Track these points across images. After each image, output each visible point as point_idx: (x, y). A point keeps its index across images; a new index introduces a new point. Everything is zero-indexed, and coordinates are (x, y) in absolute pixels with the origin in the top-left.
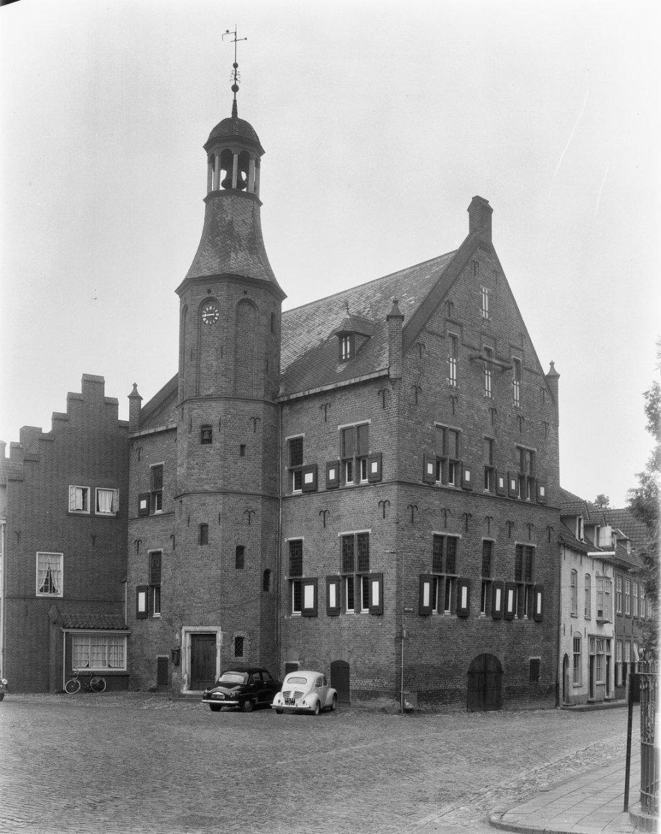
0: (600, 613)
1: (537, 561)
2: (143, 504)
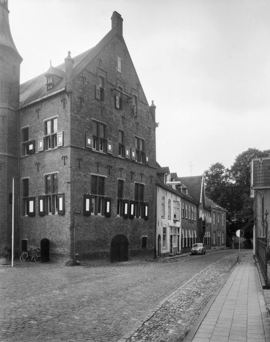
0: (175, 216)
1: (145, 191)
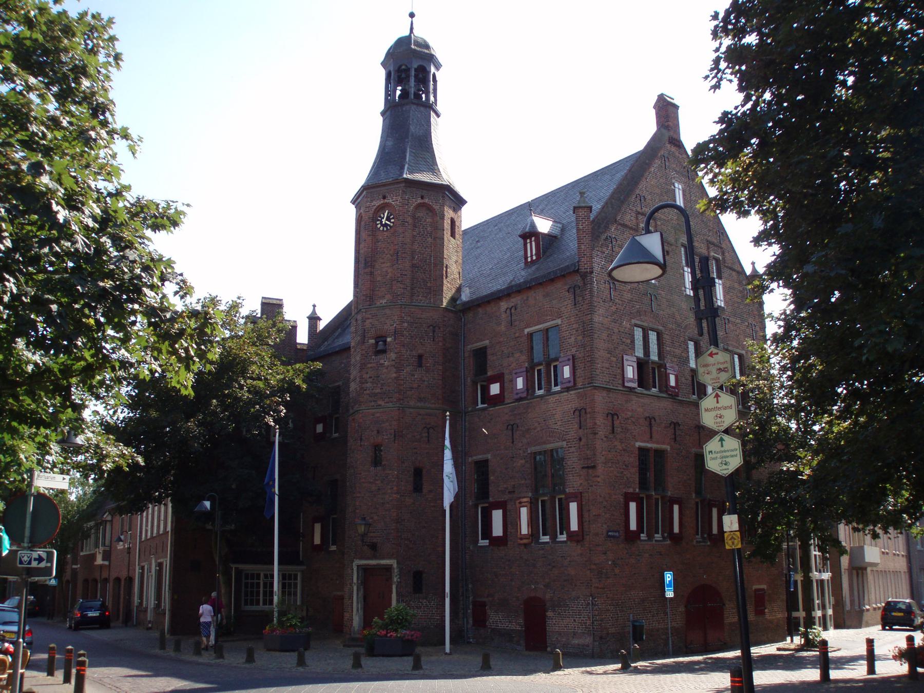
2: (320, 428)
